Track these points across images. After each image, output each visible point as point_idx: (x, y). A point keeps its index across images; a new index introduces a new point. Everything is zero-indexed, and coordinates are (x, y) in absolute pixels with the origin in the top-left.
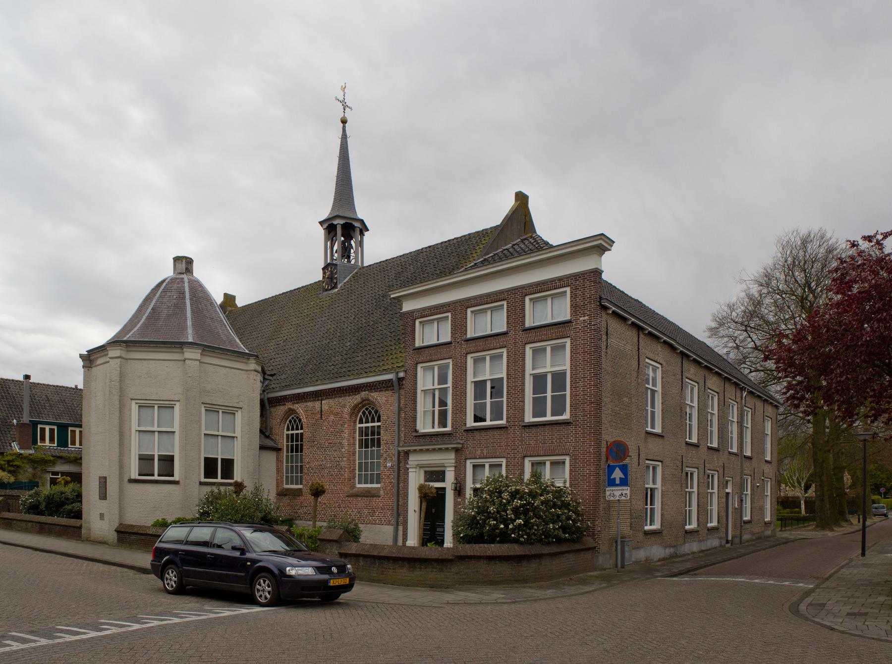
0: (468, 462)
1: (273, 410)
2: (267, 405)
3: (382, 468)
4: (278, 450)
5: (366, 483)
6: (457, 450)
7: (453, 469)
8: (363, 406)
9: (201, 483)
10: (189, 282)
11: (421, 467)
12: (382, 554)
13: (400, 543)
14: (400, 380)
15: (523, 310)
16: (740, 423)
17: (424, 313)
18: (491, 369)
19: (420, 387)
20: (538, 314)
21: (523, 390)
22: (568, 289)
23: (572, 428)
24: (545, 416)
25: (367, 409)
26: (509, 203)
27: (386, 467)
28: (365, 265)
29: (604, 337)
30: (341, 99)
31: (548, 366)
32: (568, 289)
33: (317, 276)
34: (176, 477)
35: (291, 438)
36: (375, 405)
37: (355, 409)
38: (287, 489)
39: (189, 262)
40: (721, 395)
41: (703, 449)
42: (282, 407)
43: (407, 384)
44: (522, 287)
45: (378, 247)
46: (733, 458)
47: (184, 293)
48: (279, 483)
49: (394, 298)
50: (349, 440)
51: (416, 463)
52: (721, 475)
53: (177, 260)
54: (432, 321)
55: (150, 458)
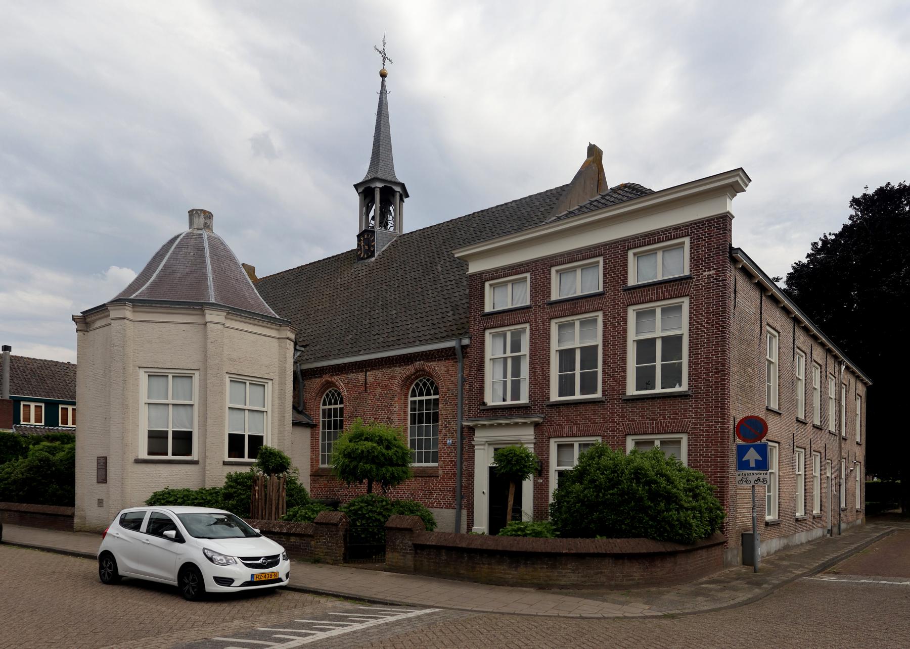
0: (552, 441)
1: (307, 383)
2: (301, 377)
3: (440, 446)
4: (313, 426)
5: (427, 461)
6: (536, 425)
7: (532, 446)
8: (417, 378)
9: (225, 463)
10: (208, 239)
11: (490, 444)
12: (472, 546)
13: (464, 530)
14: (464, 348)
15: (625, 266)
16: (838, 401)
18: (581, 335)
19: (488, 355)
20: (640, 271)
21: (624, 359)
22: (687, 240)
23: (691, 402)
24: (654, 388)
25: (421, 381)
26: (581, 158)
27: (445, 444)
28: (404, 232)
29: (733, 295)
30: (381, 49)
31: (658, 330)
32: (687, 240)
33: (352, 244)
34: (195, 456)
35: (328, 413)
36: (431, 376)
37: (407, 382)
38: (324, 470)
39: (208, 215)
40: (824, 367)
41: (809, 427)
42: (318, 380)
44: (625, 240)
45: (414, 217)
46: (832, 438)
47: (203, 250)
48: (314, 462)
49: (458, 258)
50: (399, 415)
51: (485, 440)
52: (823, 457)
53: (192, 214)
55: (162, 435)
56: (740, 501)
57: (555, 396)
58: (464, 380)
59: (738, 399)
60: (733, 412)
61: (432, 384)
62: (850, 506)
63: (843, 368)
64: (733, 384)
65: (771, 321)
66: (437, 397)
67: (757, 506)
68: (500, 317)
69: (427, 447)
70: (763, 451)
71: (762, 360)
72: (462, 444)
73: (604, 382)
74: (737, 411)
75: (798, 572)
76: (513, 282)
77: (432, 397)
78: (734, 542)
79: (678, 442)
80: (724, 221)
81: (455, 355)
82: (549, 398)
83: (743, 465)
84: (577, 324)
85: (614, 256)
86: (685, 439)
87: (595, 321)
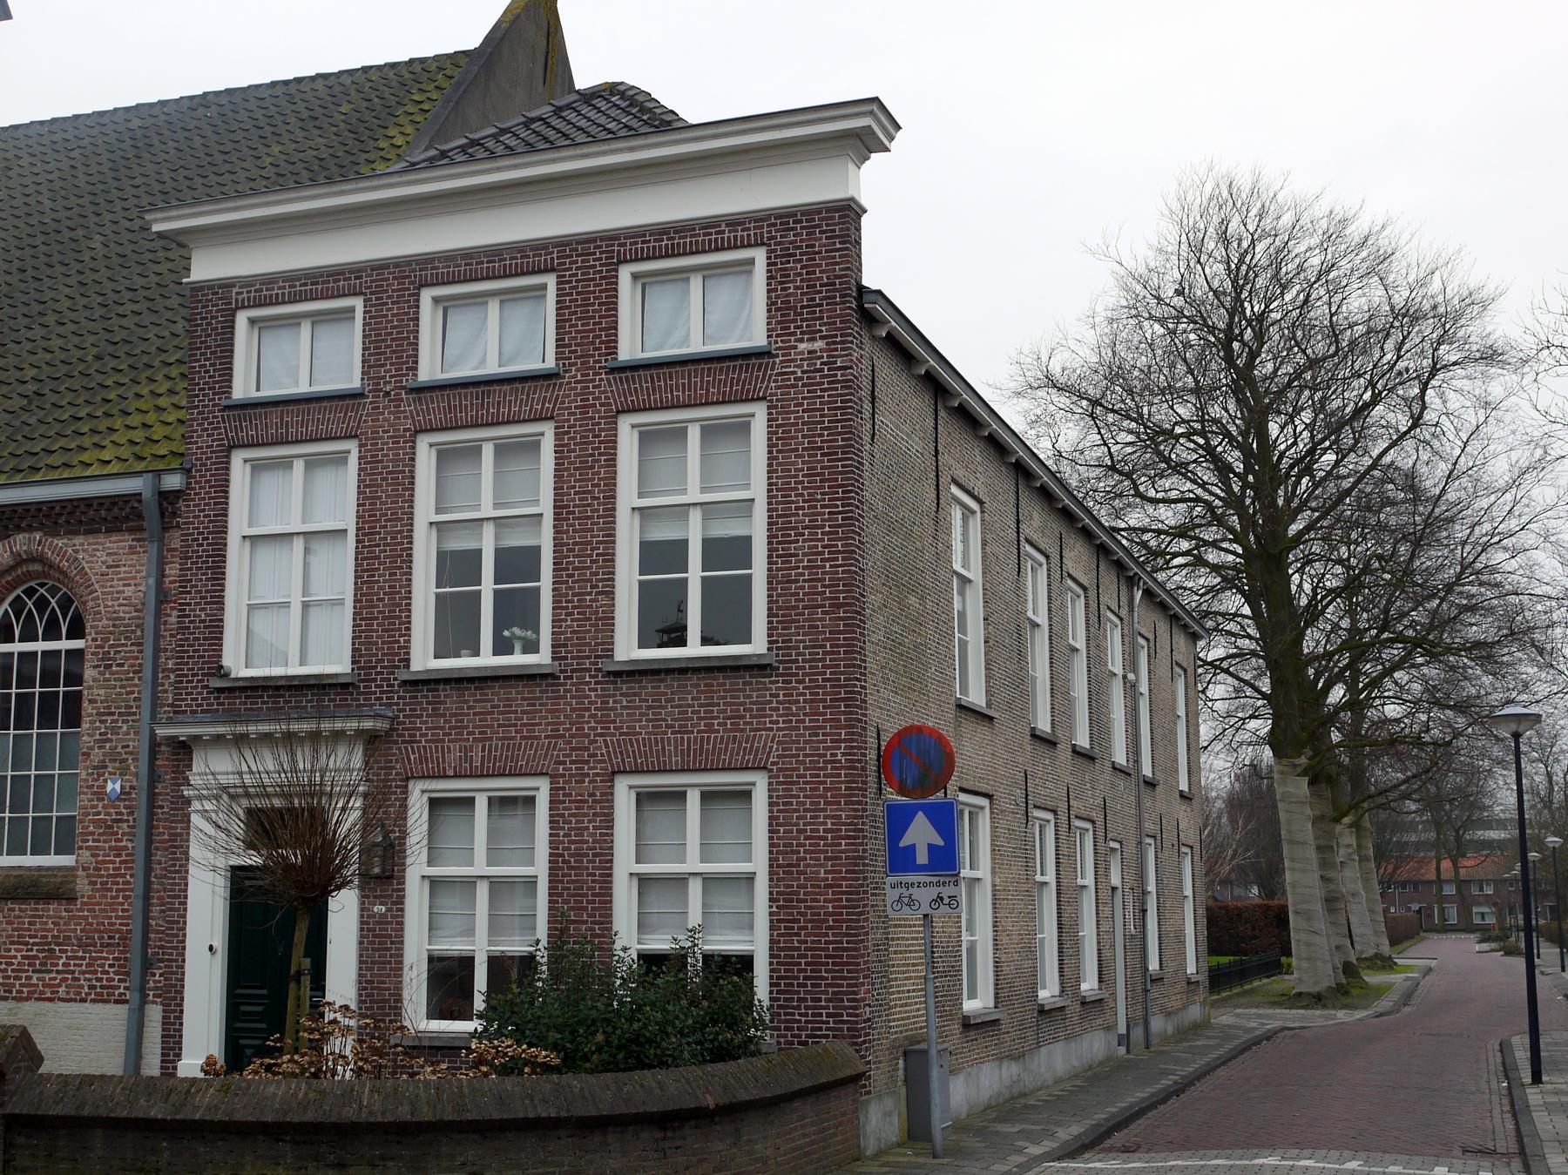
3: (84, 799)
6: (372, 740)
8: (12, 587)
13: (152, 1066)
14: (168, 499)
15: (612, 306)
17: (266, 291)
18: (492, 496)
20: (662, 321)
21: (610, 559)
23: (774, 684)
25: (30, 592)
27: (100, 794)
29: (867, 406)
43: (192, 513)
46: (1121, 782)
52: (1101, 833)
54: (294, 321)
56: (896, 959)
57: (423, 658)
58: (162, 597)
59: (885, 680)
60: (874, 715)
61: (66, 603)
62: (1171, 967)
63: (1138, 595)
64: (875, 638)
65: (960, 473)
66: (78, 644)
67: (944, 969)
68: (274, 415)
69: (43, 803)
70: (944, 819)
71: (942, 575)
72: (152, 797)
73: (556, 622)
74: (887, 714)
75: (1035, 1150)
76: (317, 318)
77: (64, 645)
78: (885, 1072)
79: (745, 795)
80: (844, 218)
81: (140, 517)
82: (407, 662)
83: (901, 860)
84: (488, 451)
85: (585, 275)
86: (760, 785)
87: (533, 446)
